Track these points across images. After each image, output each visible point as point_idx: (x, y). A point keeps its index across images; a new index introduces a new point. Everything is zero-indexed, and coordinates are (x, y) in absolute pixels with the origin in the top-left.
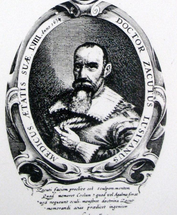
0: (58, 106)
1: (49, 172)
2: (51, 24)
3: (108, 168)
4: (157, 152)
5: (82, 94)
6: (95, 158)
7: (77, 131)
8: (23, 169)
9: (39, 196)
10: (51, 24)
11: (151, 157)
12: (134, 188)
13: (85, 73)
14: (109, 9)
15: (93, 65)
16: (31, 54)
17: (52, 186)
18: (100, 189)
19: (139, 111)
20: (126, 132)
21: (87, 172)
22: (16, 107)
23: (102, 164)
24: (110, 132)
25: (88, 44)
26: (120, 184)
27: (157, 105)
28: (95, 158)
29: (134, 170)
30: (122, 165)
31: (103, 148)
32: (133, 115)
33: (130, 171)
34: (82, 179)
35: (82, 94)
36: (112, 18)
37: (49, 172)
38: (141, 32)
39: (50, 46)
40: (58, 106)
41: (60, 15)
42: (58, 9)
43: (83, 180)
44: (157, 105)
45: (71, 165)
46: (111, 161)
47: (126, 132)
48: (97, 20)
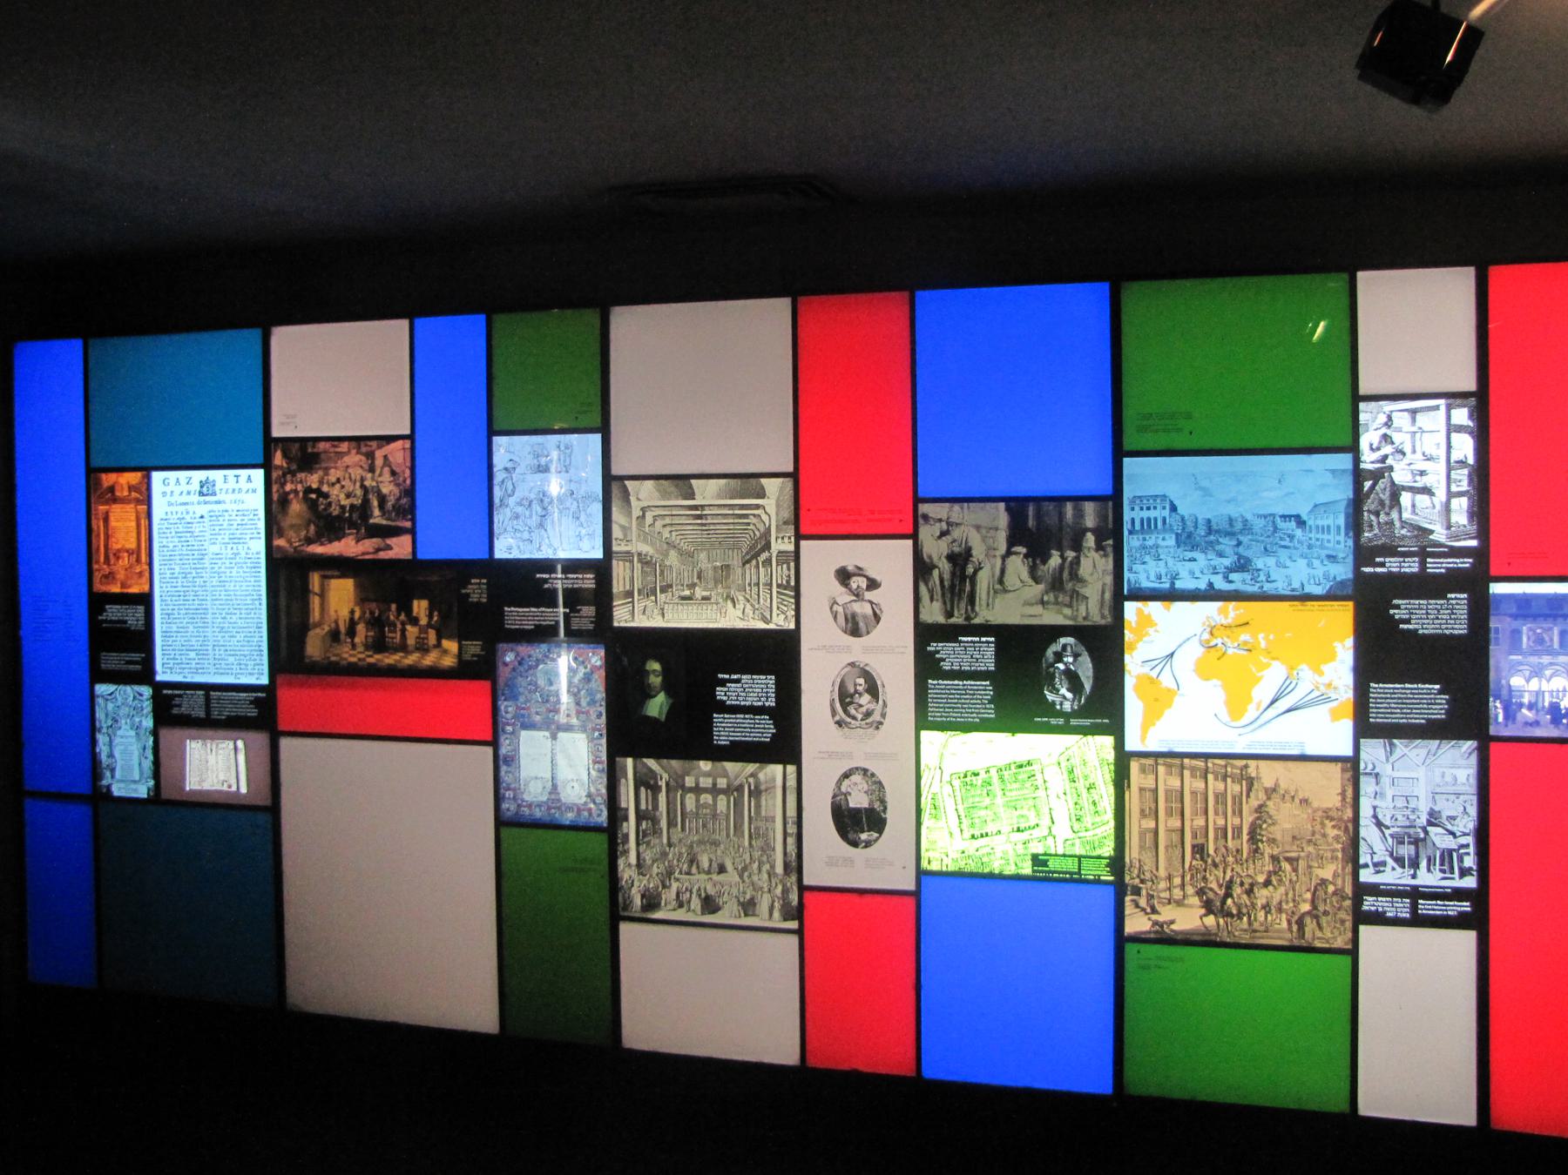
0: (848, 700)
1: (1378, 38)
2: (846, 670)
3: (867, 724)
4: (884, 718)
5: (857, 695)
6: (862, 720)
7: (855, 709)
8: (836, 723)
9: (841, 733)
10: (846, 670)
11: (882, 720)
12: (876, 732)
13: (858, 688)
14: (867, 665)
15: (861, 685)
16: (839, 681)
17: (846, 729)
18: (250, 491)
19: (877, 702)
20: (873, 710)
21: (1440, 743)
22: (833, 700)
23: (864, 722)
24: (867, 710)
25: (859, 677)
26: (871, 730)
27: (884, 701)
28: (862, 720)
29: (106, 705)
30: (871, 724)
31: (865, 716)
32: (875, 704)
33: (875, 725)
34: (857, 728)
35: (857, 695)
36: (867, 668)
37: (1378, 38)
38: (878, 674)
39: (846, 679)
40: (848, 700)
41: (850, 667)
42: (849, 664)
43: (533, 627)
44: (884, 701)
45: (853, 722)
46: (867, 721)
47: (873, 710)
48: (862, 668)
